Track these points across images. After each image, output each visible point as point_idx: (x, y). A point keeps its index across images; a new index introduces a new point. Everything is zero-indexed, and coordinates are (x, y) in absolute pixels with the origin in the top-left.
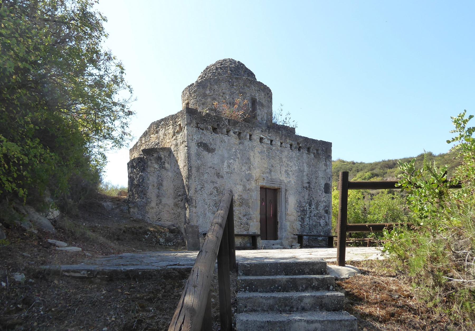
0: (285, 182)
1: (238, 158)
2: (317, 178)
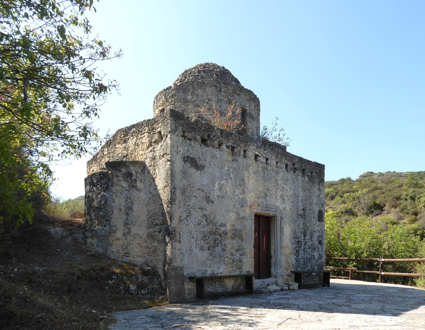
0: (281, 208)
1: (231, 178)
2: (311, 204)
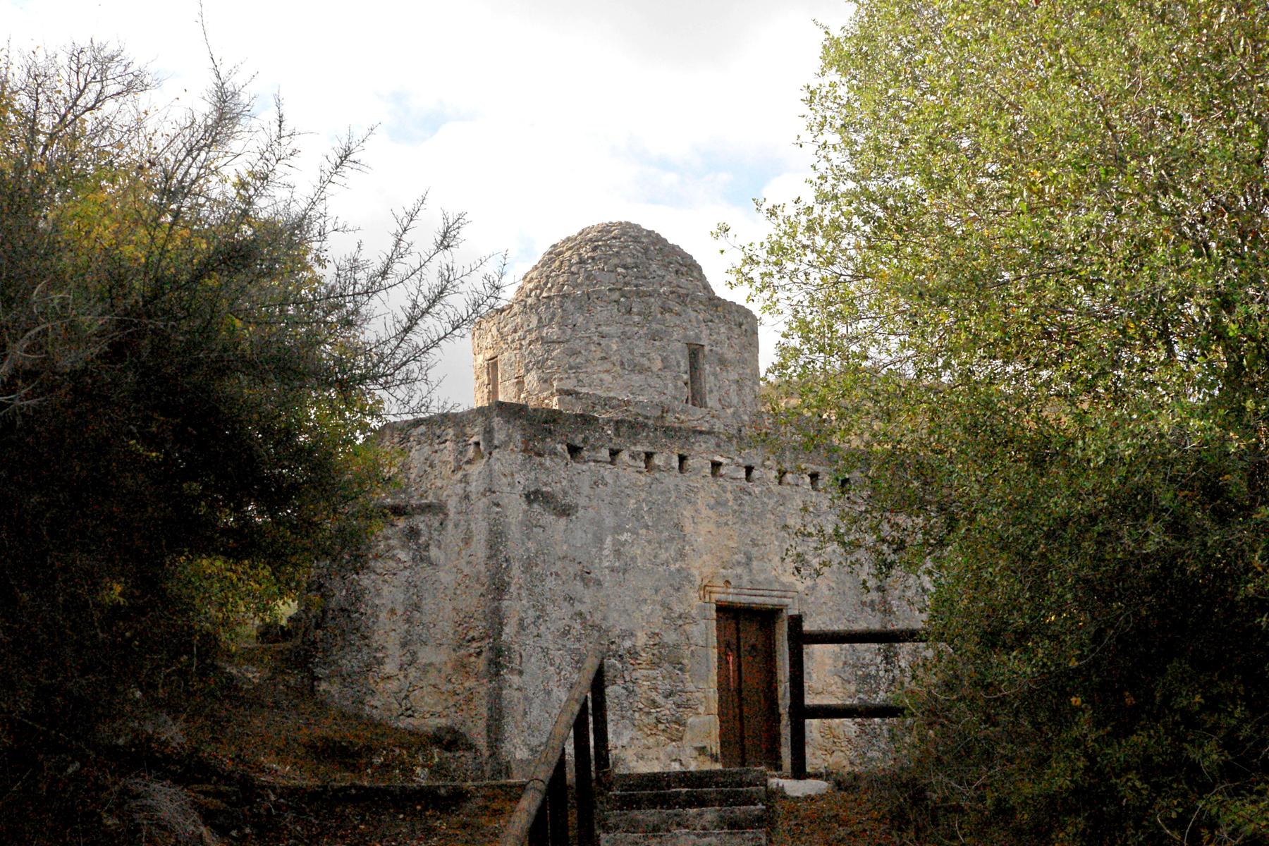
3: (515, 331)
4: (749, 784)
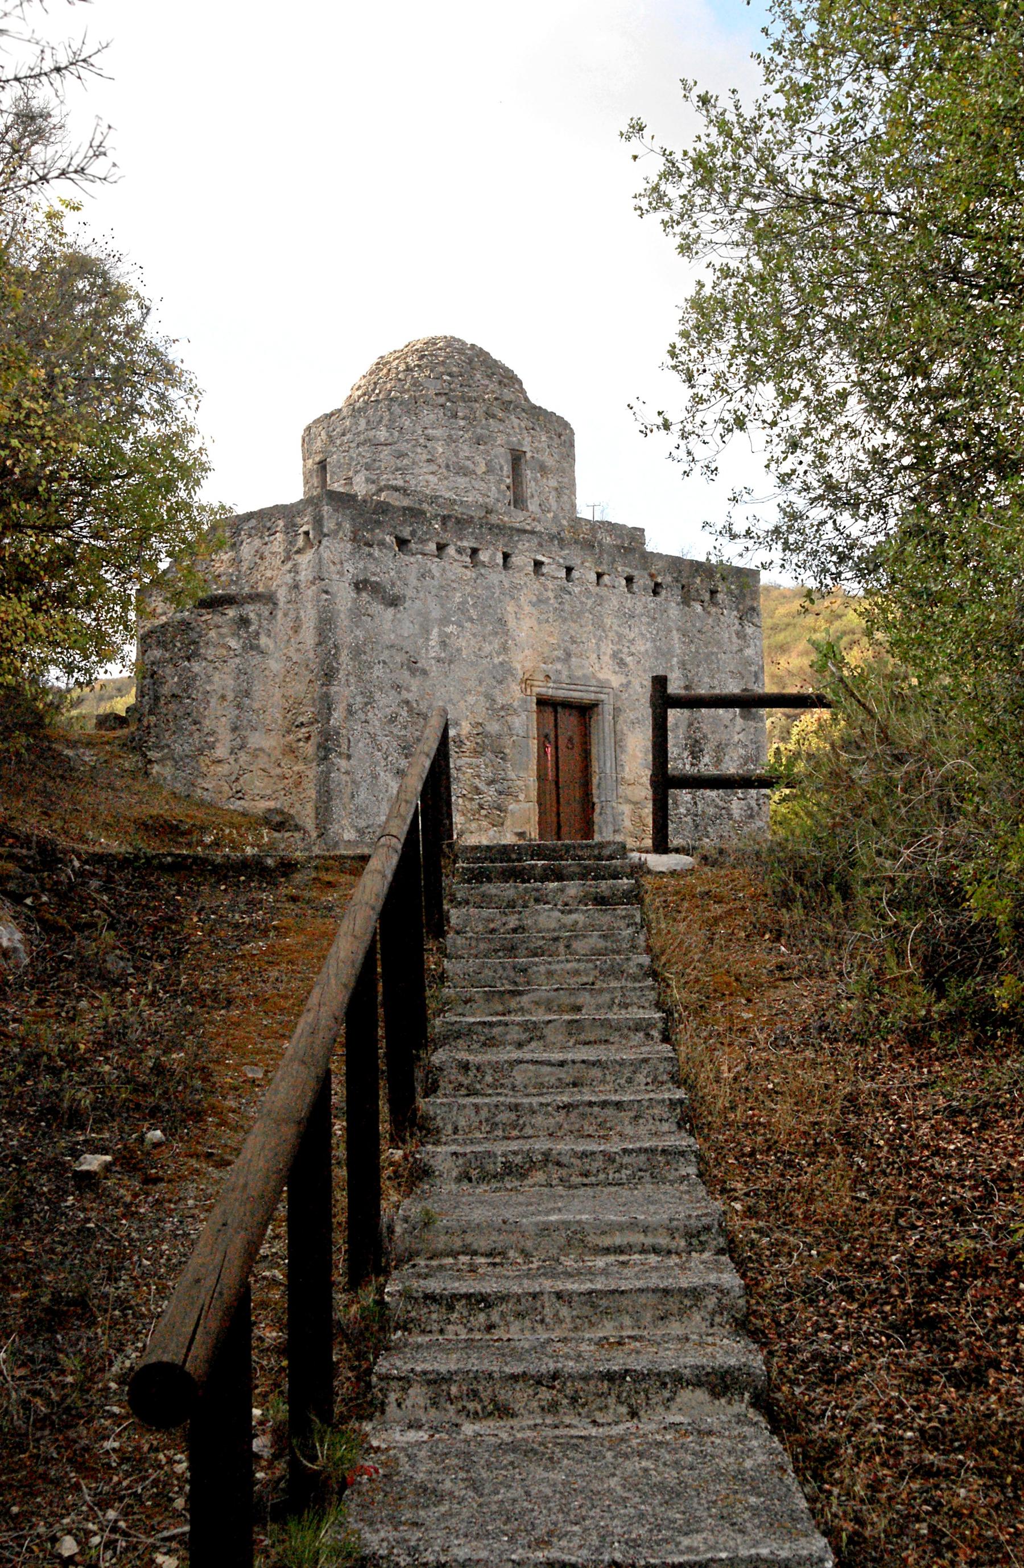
0: (615, 684)
3: (344, 435)
4: (611, 858)
